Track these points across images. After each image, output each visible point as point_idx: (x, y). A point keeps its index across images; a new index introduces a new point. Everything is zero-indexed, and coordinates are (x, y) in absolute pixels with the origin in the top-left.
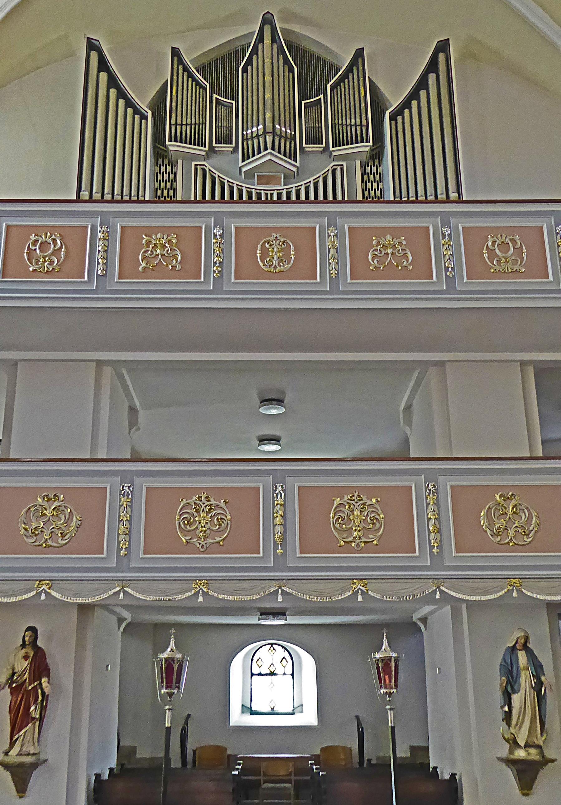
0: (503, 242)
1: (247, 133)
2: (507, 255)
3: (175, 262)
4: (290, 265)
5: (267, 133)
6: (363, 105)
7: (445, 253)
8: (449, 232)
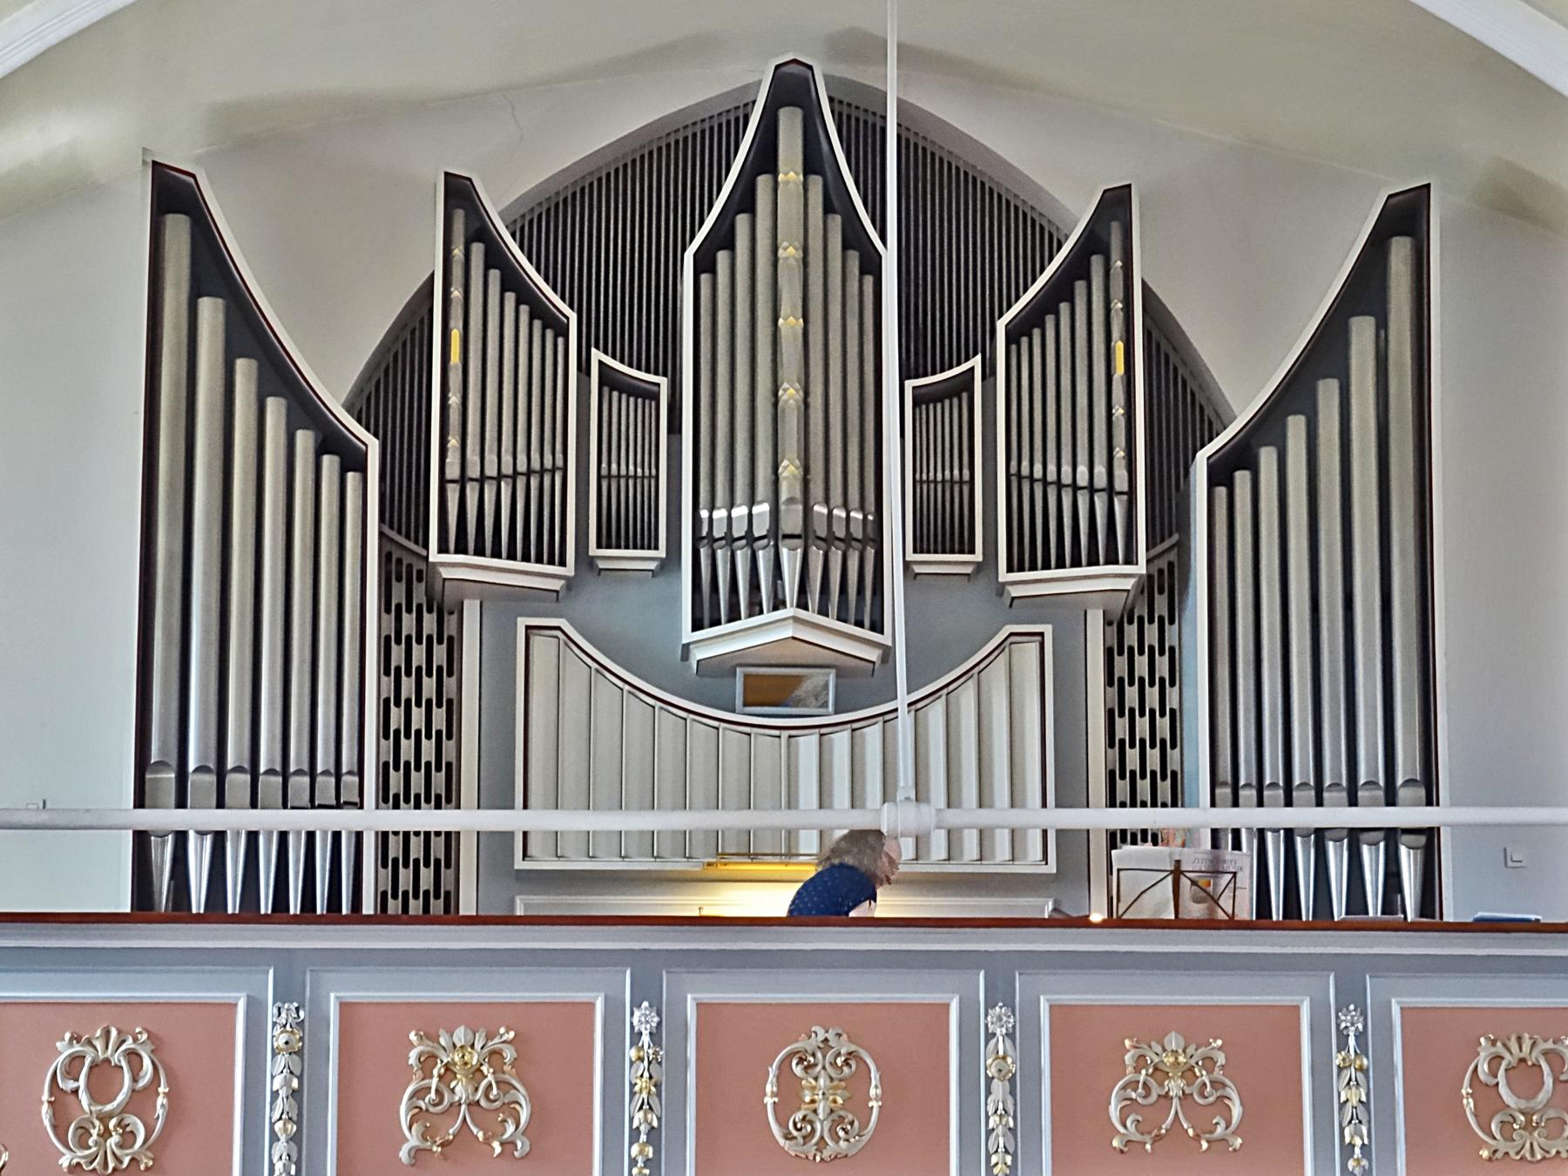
0: (1523, 1060)
1: (711, 519)
2: (1532, 1104)
3: (511, 1128)
4: (865, 1139)
5: (786, 537)
6: (1119, 411)
7: (1343, 1099)
8: (1360, 1026)
